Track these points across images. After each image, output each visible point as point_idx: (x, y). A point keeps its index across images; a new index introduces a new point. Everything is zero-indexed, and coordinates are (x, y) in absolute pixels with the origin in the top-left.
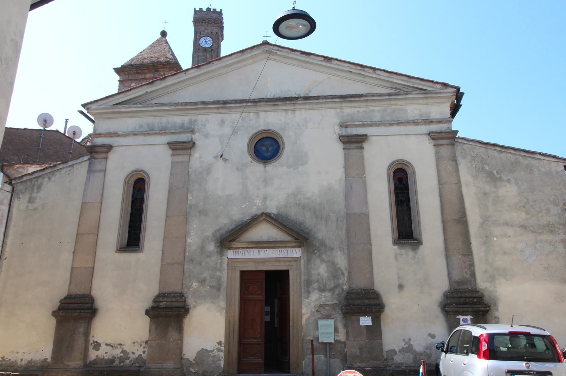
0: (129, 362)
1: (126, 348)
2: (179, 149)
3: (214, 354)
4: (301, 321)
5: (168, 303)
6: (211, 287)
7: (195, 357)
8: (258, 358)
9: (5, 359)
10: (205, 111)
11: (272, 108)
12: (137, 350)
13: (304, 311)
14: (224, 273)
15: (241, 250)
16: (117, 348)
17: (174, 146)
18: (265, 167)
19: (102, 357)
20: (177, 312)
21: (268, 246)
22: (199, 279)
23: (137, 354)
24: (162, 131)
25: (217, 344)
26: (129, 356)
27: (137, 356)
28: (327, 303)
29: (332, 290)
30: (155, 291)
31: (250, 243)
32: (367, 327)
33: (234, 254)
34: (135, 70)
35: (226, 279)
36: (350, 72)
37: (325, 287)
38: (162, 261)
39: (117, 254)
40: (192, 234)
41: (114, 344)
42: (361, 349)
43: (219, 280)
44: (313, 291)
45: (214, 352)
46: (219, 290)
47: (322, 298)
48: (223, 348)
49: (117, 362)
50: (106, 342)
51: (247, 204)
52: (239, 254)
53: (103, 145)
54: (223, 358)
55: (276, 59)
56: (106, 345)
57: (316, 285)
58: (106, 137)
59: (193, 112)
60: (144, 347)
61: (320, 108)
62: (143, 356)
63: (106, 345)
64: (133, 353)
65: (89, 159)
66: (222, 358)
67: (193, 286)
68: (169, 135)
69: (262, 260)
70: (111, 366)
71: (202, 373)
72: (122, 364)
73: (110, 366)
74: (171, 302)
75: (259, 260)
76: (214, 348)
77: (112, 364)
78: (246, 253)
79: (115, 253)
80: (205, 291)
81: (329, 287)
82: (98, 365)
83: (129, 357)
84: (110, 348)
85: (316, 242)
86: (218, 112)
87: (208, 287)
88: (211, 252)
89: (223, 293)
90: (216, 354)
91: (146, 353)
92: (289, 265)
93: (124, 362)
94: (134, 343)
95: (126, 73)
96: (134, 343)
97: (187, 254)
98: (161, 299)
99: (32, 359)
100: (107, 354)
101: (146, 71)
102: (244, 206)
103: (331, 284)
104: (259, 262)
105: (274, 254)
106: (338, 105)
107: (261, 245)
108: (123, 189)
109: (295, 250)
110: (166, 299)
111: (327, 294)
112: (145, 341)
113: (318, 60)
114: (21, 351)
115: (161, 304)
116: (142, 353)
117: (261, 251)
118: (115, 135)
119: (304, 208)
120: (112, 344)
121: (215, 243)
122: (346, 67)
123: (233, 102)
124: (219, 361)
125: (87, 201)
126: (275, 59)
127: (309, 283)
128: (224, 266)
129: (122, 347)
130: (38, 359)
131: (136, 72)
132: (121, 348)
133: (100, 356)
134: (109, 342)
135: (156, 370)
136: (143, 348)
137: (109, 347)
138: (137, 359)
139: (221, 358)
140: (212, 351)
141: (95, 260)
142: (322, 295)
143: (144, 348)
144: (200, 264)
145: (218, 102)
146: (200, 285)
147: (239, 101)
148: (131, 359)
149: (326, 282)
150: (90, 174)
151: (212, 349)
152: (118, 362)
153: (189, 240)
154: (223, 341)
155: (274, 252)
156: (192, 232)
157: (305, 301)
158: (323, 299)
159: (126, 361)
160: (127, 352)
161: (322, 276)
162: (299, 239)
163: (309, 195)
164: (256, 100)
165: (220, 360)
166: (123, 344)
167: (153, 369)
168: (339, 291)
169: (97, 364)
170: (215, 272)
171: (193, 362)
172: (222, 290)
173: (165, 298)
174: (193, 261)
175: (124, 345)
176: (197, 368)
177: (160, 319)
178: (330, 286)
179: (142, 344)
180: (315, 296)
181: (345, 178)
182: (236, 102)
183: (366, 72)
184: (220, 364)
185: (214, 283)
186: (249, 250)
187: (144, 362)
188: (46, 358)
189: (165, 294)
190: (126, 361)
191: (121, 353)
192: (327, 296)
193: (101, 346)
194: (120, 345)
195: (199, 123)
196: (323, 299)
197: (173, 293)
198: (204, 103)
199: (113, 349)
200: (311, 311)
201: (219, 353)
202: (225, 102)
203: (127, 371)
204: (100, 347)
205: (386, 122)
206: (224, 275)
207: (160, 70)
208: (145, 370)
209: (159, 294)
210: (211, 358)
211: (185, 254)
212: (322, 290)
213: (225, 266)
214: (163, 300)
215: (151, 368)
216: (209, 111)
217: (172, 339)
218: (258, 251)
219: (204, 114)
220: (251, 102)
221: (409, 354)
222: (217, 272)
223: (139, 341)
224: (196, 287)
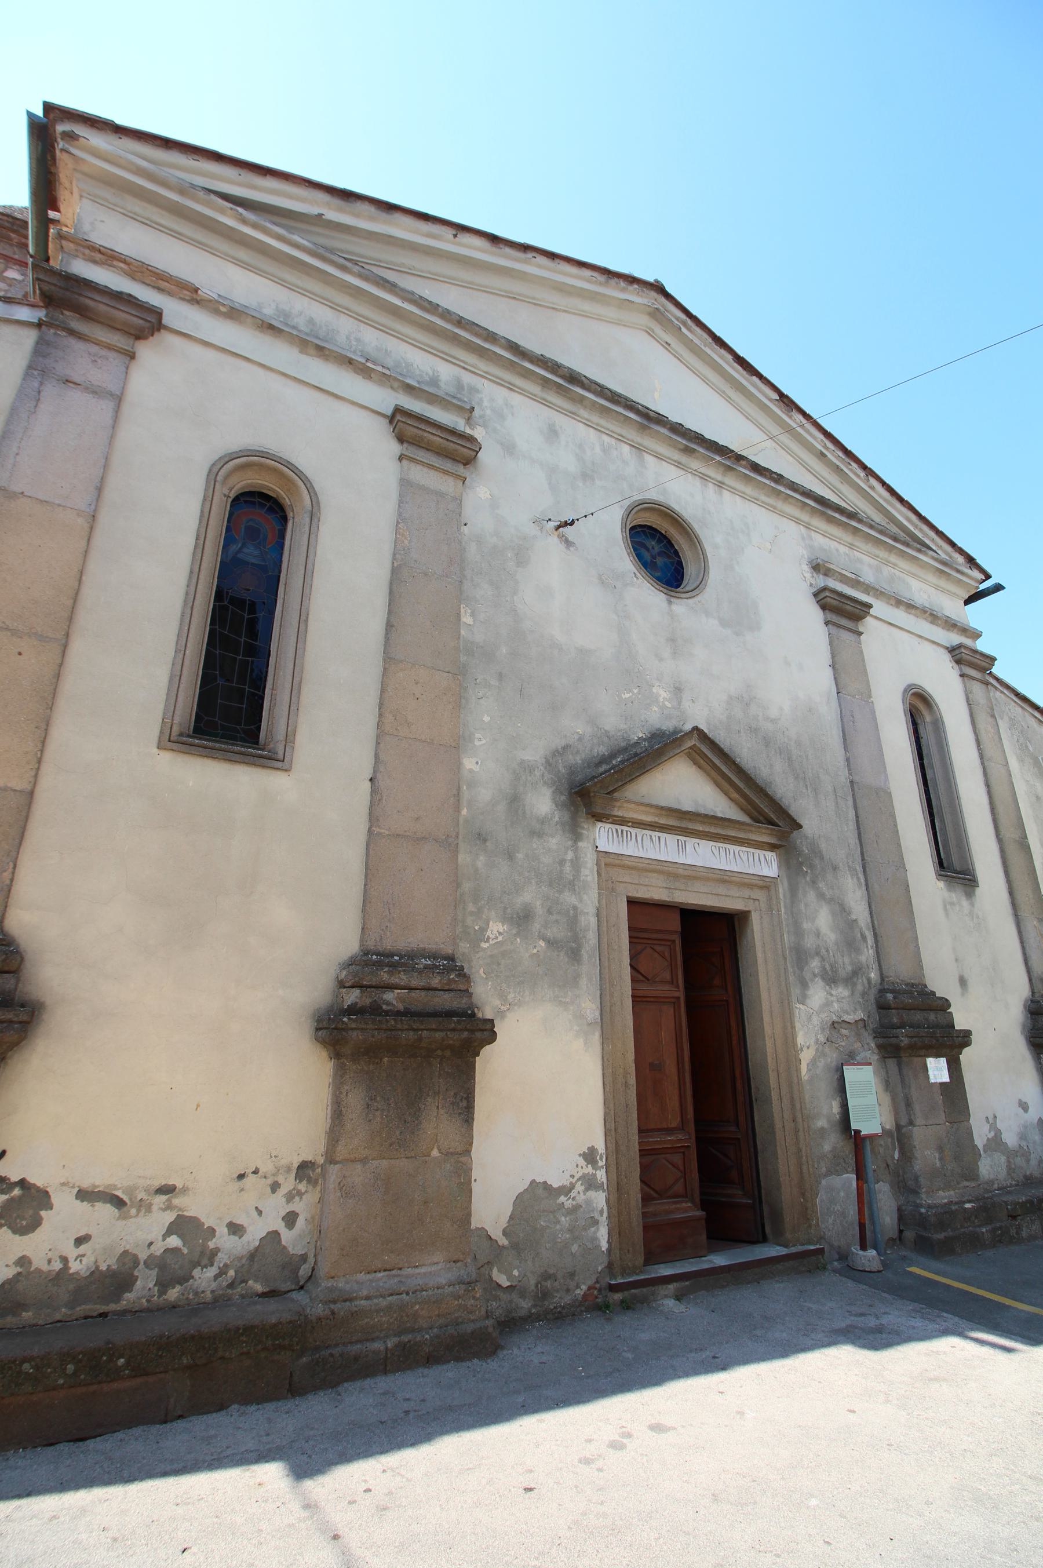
0: (216, 1277)
1: (193, 1206)
2: (428, 447)
3: (574, 1199)
4: (798, 1070)
5: (414, 994)
6: (551, 943)
7: (509, 1222)
8: (682, 1202)
10: (508, 376)
11: (677, 456)
12: (255, 1213)
13: (800, 1040)
14: (585, 897)
15: (633, 831)
16: (149, 1209)
17: (416, 431)
18: (670, 603)
19: (57, 1266)
20: (465, 1034)
21: (707, 830)
22: (509, 911)
23: (256, 1232)
24: (374, 363)
25: (582, 1162)
26: (211, 1245)
28: (847, 1018)
29: (849, 980)
30: (350, 945)
31: (663, 812)
32: (942, 1084)
33: (613, 841)
35: (593, 920)
36: (823, 454)
37: (836, 972)
38: (373, 819)
39: (166, 756)
40: (477, 743)
41: (131, 1190)
42: (940, 1149)
43: (573, 919)
44: (812, 980)
45: (572, 1194)
46: (575, 955)
47: (832, 1002)
48: (601, 1175)
49: (145, 1283)
50: (86, 1184)
51: (636, 691)
52: (629, 843)
53: (130, 295)
54: (605, 1214)
55: (669, 345)
56: (84, 1195)
57: (815, 964)
58: (134, 279)
59: (471, 359)
60: (290, 1192)
61: (772, 506)
62: (287, 1237)
63: (84, 1195)
64: (235, 1229)
65: (39, 325)
66: (601, 1212)
67: (489, 933)
68: (392, 388)
69: (686, 873)
70: (113, 1307)
71: (537, 1286)
72: (173, 1294)
73: (103, 1308)
74: (423, 989)
75: (681, 871)
76: (572, 1176)
77: (118, 1299)
78: (647, 842)
79: (155, 751)
80: (532, 956)
81: (842, 973)
82: (27, 1315)
83: (215, 1252)
84: (105, 1211)
85: (801, 842)
86: (541, 398)
87: (542, 943)
88: (543, 821)
89: (589, 968)
90: (581, 1198)
91: (300, 1222)
92: (749, 898)
93: (184, 1279)
94: (241, 1177)
96: (241, 1177)
97: (464, 812)
98: (384, 976)
100: (83, 1248)
102: (627, 696)
103: (845, 965)
104: (676, 876)
105: (718, 858)
106: (805, 517)
107: (691, 826)
108: (205, 499)
109: (764, 855)
110: (403, 976)
111: (841, 993)
112: (296, 1165)
113: (766, 397)
115: (389, 996)
116: (279, 1226)
117: (685, 841)
118: (190, 294)
119: (767, 741)
120: (119, 1193)
121: (553, 792)
122: (818, 440)
123: (593, 386)
124: (593, 1229)
125: (16, 488)
126: (667, 343)
127: (801, 957)
128: (587, 876)
129: (176, 1202)
132: (169, 1207)
133: (39, 1262)
134: (98, 1178)
135: (383, 1303)
136: (284, 1200)
137: (99, 1205)
138: (253, 1256)
139: (596, 1215)
140: (566, 1190)
141: (39, 761)
142: (832, 995)
143: (290, 1197)
144: (510, 856)
145: (554, 367)
146: (514, 931)
147: (609, 393)
148: (222, 1259)
149: (834, 957)
150: (41, 383)
151: (565, 1181)
152: (151, 1285)
153: (469, 763)
154: (601, 1147)
155: (716, 852)
156: (477, 735)
157: (800, 1011)
158: (836, 1005)
159: (196, 1272)
160: (203, 1224)
161: (825, 939)
162: (780, 824)
163: (773, 713)
164: (652, 414)
165: (596, 1223)
166: (179, 1185)
167: (368, 1298)
168: (863, 984)
169: (19, 1306)
170: (561, 892)
171: (500, 1243)
172: (585, 956)
173: (399, 972)
174: (485, 840)
175: (185, 1190)
176: (518, 1268)
177: (386, 1059)
178: (844, 969)
179: (280, 1179)
180: (818, 994)
181: (838, 693)
182: (601, 391)
183: (851, 470)
184: (595, 1239)
185: (558, 932)
186: (655, 834)
187: (291, 1264)
189: (392, 955)
190: (196, 1272)
191: (165, 1236)
192: (843, 998)
193: (49, 1206)
194: (167, 1190)
195: (486, 403)
196: (836, 1005)
197: (424, 954)
198: (514, 348)
199: (125, 1217)
200: (817, 1041)
201: (591, 1194)
202: (574, 378)
203: (248, 1329)
204: (43, 1213)
205: (893, 594)
206: (589, 902)
208: (333, 1313)
209: (366, 953)
210: (563, 1219)
211: (458, 810)
212: (831, 979)
213: (589, 873)
214: (394, 980)
215: (356, 1298)
216: (519, 381)
217: (439, 1150)
218: (678, 840)
219: (499, 383)
220: (638, 412)
221: (1000, 1154)
222: (567, 893)
223: (267, 1167)
224: (500, 938)
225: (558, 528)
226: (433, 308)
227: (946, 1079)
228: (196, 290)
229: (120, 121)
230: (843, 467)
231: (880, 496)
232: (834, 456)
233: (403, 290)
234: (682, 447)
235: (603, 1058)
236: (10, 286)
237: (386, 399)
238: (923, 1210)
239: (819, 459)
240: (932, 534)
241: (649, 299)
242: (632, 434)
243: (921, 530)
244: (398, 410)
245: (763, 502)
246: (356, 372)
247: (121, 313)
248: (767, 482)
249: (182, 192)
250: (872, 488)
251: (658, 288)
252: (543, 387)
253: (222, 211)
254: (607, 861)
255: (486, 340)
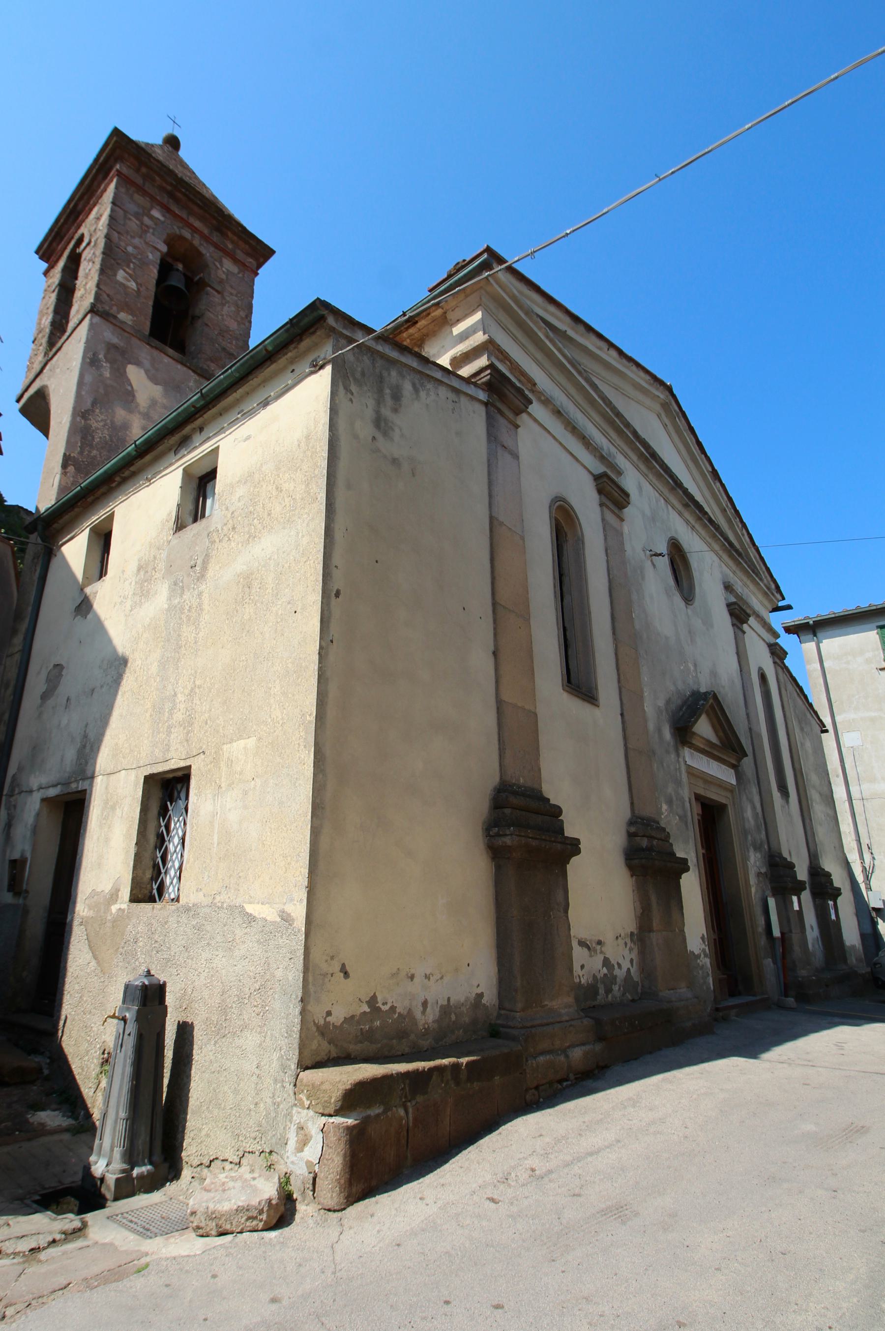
9: (380, 1005)
27: (625, 974)
32: (797, 911)
34: (171, 184)
36: (725, 510)
55: (667, 426)
61: (709, 543)
68: (595, 456)
95: (144, 170)
99: (372, 1001)
101: (196, 209)
113: (706, 468)
114: (419, 972)
130: (462, 1000)
131: (169, 188)
160: (611, 962)
183: (735, 522)
188: (479, 991)
198: (635, 433)
207: (230, 234)
225: (652, 556)
226: (609, 403)
227: (798, 909)
228: (535, 384)
229: (543, 287)
230: (732, 520)
231: (746, 541)
232: (730, 512)
233: (600, 391)
234: (684, 503)
235: (701, 885)
236: (156, 224)
237: (600, 468)
238: (800, 979)
239: (722, 512)
240: (764, 568)
241: (662, 395)
242: (666, 492)
243: (759, 565)
244: (605, 475)
245: (707, 541)
246: (583, 444)
247: (518, 401)
248: (713, 529)
249: (527, 314)
250: (743, 535)
251: (669, 389)
252: (639, 457)
253: (540, 328)
254: (692, 772)
255: (625, 426)
